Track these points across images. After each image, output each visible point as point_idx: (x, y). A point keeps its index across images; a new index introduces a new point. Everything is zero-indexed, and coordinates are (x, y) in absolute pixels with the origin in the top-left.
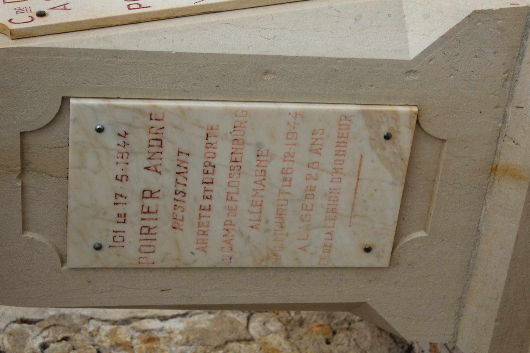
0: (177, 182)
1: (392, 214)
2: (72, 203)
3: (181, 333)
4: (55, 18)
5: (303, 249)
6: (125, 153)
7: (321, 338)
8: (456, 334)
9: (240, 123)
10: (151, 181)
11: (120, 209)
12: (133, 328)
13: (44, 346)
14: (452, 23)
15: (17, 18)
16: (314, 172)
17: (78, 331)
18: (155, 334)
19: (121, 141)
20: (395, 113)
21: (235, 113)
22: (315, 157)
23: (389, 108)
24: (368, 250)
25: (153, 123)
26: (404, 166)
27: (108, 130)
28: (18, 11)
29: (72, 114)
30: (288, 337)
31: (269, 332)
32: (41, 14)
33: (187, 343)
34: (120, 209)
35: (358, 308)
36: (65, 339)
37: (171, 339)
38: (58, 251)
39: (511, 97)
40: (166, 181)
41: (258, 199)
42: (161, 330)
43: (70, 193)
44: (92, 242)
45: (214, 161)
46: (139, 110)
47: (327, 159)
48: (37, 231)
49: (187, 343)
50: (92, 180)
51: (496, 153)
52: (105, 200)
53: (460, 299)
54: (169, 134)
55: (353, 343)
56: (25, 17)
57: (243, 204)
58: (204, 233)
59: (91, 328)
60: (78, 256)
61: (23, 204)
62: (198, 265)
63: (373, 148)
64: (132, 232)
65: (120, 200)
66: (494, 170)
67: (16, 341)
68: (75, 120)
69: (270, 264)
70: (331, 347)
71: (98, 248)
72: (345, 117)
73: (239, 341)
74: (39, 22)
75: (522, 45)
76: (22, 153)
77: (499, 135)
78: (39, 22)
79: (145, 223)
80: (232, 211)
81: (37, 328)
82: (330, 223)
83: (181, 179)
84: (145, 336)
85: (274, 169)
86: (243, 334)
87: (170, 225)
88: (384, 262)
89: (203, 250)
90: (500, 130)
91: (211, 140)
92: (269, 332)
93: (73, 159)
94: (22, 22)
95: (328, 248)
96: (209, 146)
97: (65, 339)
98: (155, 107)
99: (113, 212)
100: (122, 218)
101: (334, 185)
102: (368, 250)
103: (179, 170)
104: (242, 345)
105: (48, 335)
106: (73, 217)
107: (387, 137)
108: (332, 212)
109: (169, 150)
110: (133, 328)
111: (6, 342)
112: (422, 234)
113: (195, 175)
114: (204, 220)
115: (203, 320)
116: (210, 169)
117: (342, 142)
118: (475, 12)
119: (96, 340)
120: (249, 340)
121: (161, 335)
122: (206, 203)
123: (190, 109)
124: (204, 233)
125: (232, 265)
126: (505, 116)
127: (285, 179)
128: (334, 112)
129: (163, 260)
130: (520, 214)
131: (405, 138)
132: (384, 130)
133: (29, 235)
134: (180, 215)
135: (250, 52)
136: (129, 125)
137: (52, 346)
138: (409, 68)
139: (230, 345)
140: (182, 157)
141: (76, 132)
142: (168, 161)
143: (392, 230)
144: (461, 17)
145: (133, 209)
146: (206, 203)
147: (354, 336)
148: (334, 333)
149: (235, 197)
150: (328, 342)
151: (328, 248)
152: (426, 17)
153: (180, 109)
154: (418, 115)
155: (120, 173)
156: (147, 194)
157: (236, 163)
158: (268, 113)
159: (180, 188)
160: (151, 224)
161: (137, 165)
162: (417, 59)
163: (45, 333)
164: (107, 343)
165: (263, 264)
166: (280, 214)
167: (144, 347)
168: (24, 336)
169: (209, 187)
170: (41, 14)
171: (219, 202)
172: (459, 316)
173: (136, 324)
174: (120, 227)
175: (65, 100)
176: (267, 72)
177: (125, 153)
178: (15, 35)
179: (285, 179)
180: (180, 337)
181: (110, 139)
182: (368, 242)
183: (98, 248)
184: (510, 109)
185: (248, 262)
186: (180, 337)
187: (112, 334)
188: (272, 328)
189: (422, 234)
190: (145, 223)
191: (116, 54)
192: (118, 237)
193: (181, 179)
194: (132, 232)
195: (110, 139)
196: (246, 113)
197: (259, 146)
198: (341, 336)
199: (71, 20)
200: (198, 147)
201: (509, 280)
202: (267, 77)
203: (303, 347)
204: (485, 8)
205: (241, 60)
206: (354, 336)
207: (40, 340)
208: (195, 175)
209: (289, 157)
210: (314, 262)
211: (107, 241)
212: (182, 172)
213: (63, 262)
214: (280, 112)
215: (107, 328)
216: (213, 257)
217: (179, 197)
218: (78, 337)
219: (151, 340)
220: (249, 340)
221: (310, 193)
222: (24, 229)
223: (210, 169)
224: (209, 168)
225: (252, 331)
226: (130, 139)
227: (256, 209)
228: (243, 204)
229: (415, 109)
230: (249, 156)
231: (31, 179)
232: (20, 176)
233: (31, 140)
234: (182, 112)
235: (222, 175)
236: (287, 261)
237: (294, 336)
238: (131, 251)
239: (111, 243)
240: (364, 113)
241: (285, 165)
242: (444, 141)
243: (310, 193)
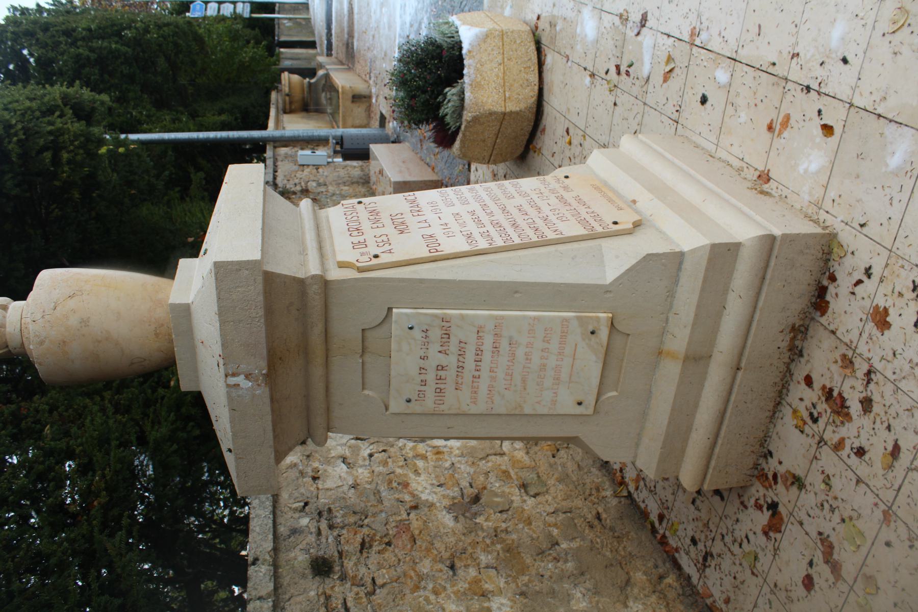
0: (459, 361)
1: (595, 382)
2: (393, 373)
3: (458, 449)
4: (385, 259)
5: (538, 403)
6: (426, 344)
7: (549, 453)
8: (636, 456)
9: (499, 324)
10: (442, 359)
11: (423, 377)
12: (427, 445)
13: (371, 455)
14: (634, 261)
15: (361, 259)
16: (545, 354)
17: (392, 446)
18: (442, 449)
19: (424, 334)
20: (598, 317)
21: (496, 317)
22: (547, 345)
23: (594, 314)
24: (580, 404)
25: (444, 324)
26: (603, 351)
27: (416, 328)
28: (362, 254)
29: (394, 318)
30: (527, 453)
31: (516, 449)
32: (376, 256)
33: (462, 455)
34: (423, 377)
35: (571, 441)
36: (384, 451)
37: (451, 452)
38: (384, 402)
39: (671, 308)
40: (451, 360)
41: (510, 372)
42: (445, 446)
43: (392, 367)
44: (405, 398)
45: (482, 348)
46: (435, 316)
47: (554, 346)
48: (371, 390)
49: (462, 455)
50: (405, 358)
51: (662, 342)
52: (414, 371)
53: (639, 434)
54: (454, 331)
55: (570, 457)
56: (366, 258)
57: (501, 374)
58: (475, 392)
59: (400, 445)
60: (397, 405)
61: (363, 373)
62: (471, 412)
63: (584, 340)
64: (430, 391)
65: (423, 371)
66: (660, 353)
67: (353, 451)
68: (396, 322)
69: (517, 412)
70: (556, 459)
71: (409, 401)
72: (565, 320)
73: (495, 455)
74: (375, 261)
75: (678, 275)
76: (363, 341)
77: (663, 332)
78: (375, 261)
79: (438, 386)
80: (493, 379)
81: (366, 443)
82: (556, 387)
83: (461, 359)
84: (435, 450)
85: (520, 353)
86: (499, 450)
87: (454, 387)
88: (590, 411)
89: (475, 403)
90: (664, 328)
91: (480, 334)
92: (516, 449)
93: (394, 346)
94: (365, 261)
95: (554, 402)
96: (479, 338)
97: (384, 451)
98: (445, 314)
99: (418, 379)
100: (424, 383)
101: (558, 363)
102: (580, 404)
103: (460, 353)
104: (498, 457)
105: (373, 448)
106: (393, 382)
107: (593, 333)
108: (557, 379)
109: (454, 341)
110: (427, 445)
111: (347, 452)
112: (614, 393)
113: (470, 356)
114: (475, 384)
115: (473, 443)
116: (480, 353)
117: (564, 336)
118: (648, 255)
119: (404, 452)
120: (502, 454)
121: (445, 450)
122: (477, 374)
123: (467, 315)
124: (475, 392)
125: (493, 412)
126: (667, 319)
127: (527, 359)
128: (559, 317)
129: (449, 409)
130: (676, 381)
131: (604, 333)
132: (591, 328)
133: (366, 392)
134: (460, 381)
135: (506, 279)
136: (429, 325)
137: (376, 455)
138: (606, 290)
139: (490, 457)
140: (462, 345)
141: (396, 329)
142: (453, 347)
143: (595, 391)
144: (639, 258)
145: (431, 377)
146: (477, 374)
147: (571, 452)
148: (558, 450)
149: (495, 370)
150: (554, 457)
151: (554, 402)
152: (617, 257)
153: (462, 315)
154: (612, 319)
155: (423, 355)
156: (440, 368)
157: (496, 348)
158: (516, 317)
159: (461, 364)
160: (442, 386)
161: (434, 348)
162: (612, 284)
163: (371, 447)
164: (410, 455)
165: (513, 412)
166: (524, 381)
167: (434, 457)
168: (359, 449)
169: (479, 363)
170: (376, 256)
171: (485, 374)
172: (637, 445)
173: (429, 442)
174: (423, 388)
175: (390, 310)
176: (516, 292)
177: (426, 344)
178: (361, 270)
179: (527, 359)
180: (457, 452)
181: (417, 334)
182: (580, 399)
183: (409, 401)
184: (671, 315)
185: (503, 411)
186: (457, 452)
187: (414, 448)
188: (518, 447)
189: (614, 393)
190: (438, 386)
191: (421, 281)
192: (421, 395)
193: (461, 359)
194: (430, 391)
195: (417, 334)
196: (502, 317)
197: (511, 338)
198: (562, 453)
199: (394, 260)
200: (472, 339)
201: (669, 423)
202: (517, 295)
203: (537, 459)
204: (654, 252)
205: (500, 285)
206: (571, 452)
207: (368, 451)
208: (470, 356)
209: (529, 345)
210: (545, 411)
211: (414, 397)
212: (461, 354)
213: (387, 409)
214: (525, 317)
215: (410, 444)
216: (481, 408)
217: (460, 370)
218: (392, 450)
219: (438, 453)
220: (502, 454)
221: (543, 367)
222: (363, 389)
223: (480, 353)
224: (479, 352)
225: (504, 449)
226: (429, 333)
227: (509, 378)
228: (501, 374)
229: (610, 315)
230: (504, 344)
231: (368, 358)
232: (362, 356)
233: (368, 334)
234: (462, 317)
235: (487, 357)
236: (527, 410)
237: (532, 452)
238: (429, 403)
239: (417, 398)
240: (578, 318)
241: (527, 350)
242: (628, 335)
243: (543, 367)
